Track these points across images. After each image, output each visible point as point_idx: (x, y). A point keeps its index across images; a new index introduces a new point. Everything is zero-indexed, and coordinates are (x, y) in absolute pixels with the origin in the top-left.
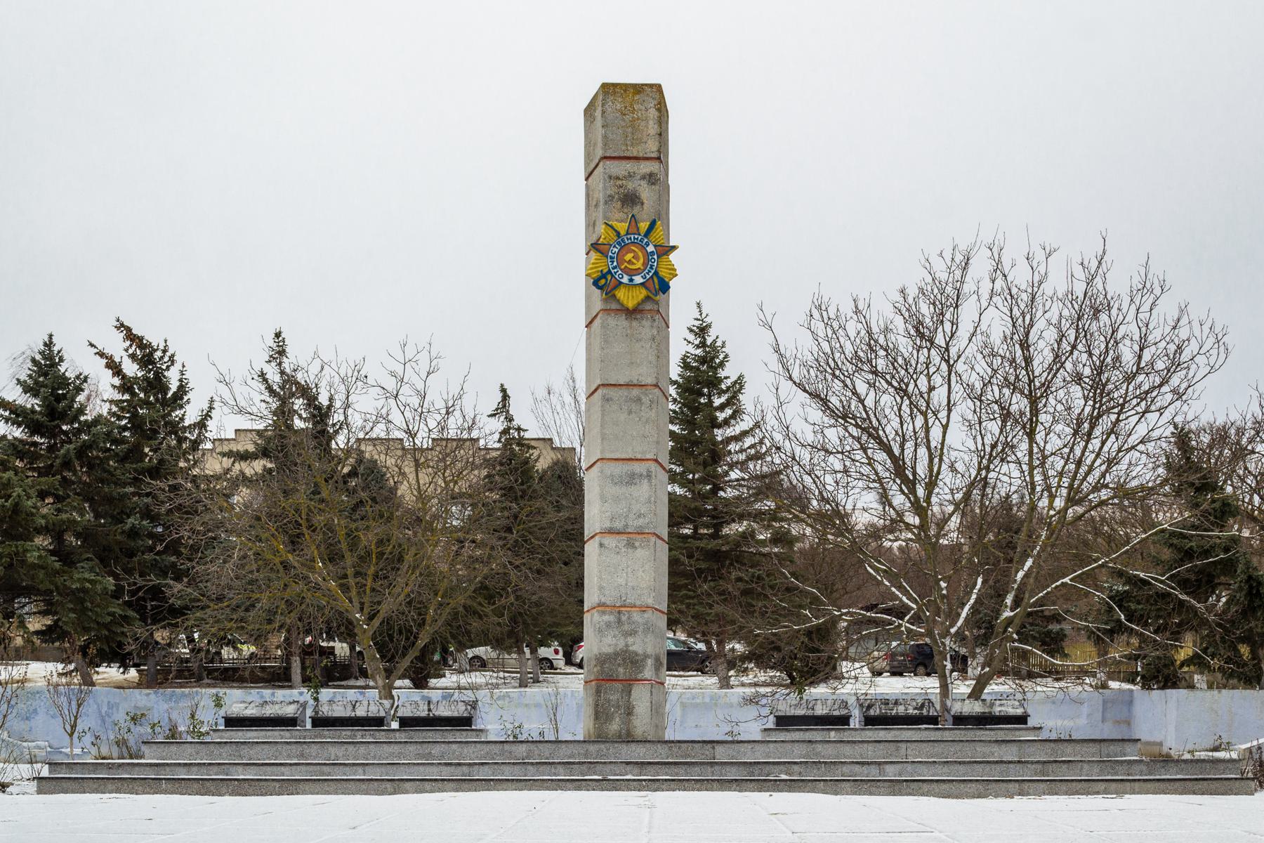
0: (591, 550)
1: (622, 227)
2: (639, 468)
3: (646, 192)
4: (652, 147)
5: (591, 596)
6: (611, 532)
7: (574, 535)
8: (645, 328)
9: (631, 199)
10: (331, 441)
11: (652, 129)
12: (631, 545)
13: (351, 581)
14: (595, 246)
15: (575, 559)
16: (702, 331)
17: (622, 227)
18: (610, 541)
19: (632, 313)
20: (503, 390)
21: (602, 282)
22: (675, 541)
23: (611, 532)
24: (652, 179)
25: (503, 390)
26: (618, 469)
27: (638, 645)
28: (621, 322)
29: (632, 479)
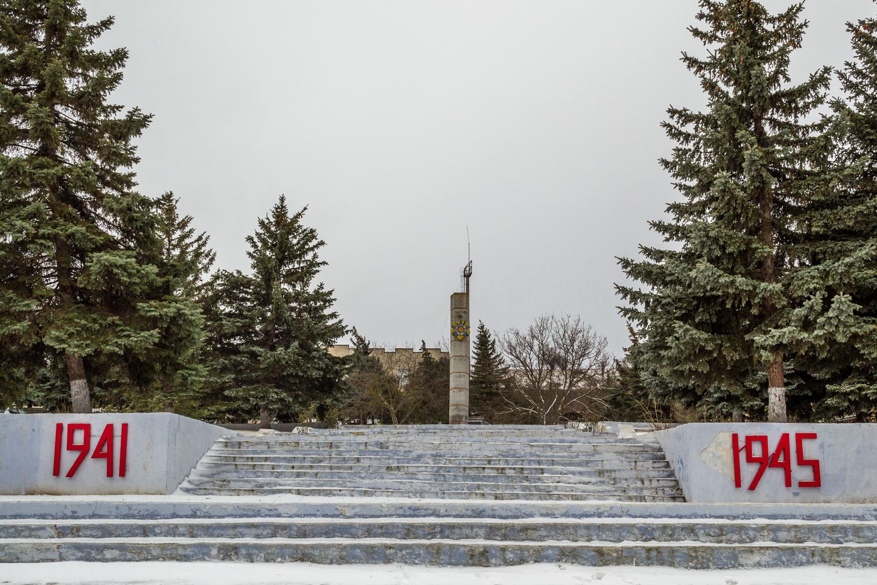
0: (451, 392)
1: (458, 323)
2: (462, 374)
3: (464, 315)
4: (465, 306)
5: (451, 403)
6: (455, 388)
7: (447, 386)
8: (464, 344)
9: (460, 317)
10: (19, 130)
11: (465, 302)
12: (460, 391)
13: (391, 399)
14: (452, 327)
15: (447, 395)
16: (482, 327)
17: (458, 323)
18: (455, 390)
19: (460, 341)
20: (423, 341)
21: (454, 334)
22: (471, 391)
23: (455, 388)
24: (465, 312)
25: (423, 341)
26: (457, 374)
27: (461, 413)
28: (458, 343)
29: (460, 376)
